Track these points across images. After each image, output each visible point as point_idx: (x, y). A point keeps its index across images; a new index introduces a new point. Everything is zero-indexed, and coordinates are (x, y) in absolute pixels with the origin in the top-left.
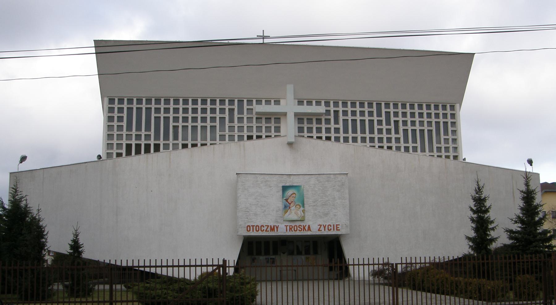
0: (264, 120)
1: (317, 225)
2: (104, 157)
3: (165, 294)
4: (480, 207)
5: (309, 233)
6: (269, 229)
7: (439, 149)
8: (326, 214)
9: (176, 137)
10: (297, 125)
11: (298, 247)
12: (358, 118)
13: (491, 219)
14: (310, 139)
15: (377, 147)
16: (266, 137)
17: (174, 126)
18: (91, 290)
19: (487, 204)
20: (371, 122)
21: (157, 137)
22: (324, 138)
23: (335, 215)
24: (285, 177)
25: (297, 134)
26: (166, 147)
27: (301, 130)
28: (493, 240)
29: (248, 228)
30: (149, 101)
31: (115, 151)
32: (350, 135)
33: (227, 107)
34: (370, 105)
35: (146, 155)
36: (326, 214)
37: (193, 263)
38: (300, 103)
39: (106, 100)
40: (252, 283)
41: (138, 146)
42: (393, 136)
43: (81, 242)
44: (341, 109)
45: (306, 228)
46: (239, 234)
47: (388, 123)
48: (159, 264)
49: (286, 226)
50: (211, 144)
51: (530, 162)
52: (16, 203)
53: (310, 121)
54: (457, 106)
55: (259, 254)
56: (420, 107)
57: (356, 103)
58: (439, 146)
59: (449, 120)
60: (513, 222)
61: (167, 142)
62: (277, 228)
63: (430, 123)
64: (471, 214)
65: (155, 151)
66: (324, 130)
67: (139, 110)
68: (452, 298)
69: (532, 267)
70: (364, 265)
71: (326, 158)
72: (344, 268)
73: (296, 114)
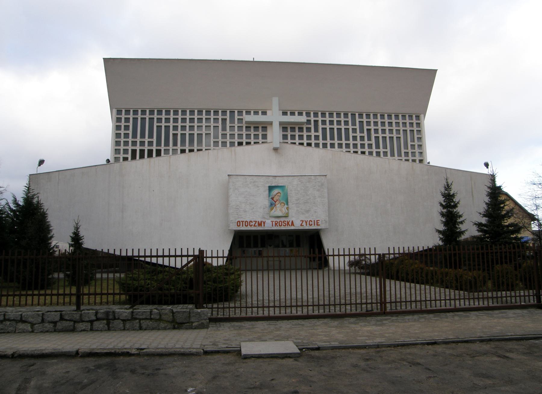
0: (252, 129)
1: (299, 221)
2: (112, 161)
3: (148, 284)
4: (449, 203)
5: (292, 228)
6: (257, 224)
7: (407, 154)
8: (308, 211)
9: (175, 144)
10: (282, 133)
11: (282, 241)
12: (335, 127)
13: (460, 214)
14: (294, 145)
15: (352, 152)
16: (255, 143)
17: (174, 134)
18: (93, 278)
19: (456, 199)
20: (347, 130)
21: (159, 143)
22: (305, 144)
23: (315, 212)
24: (271, 178)
25: (282, 141)
26: (167, 152)
27: (285, 137)
28: (462, 233)
29: (239, 223)
30: (152, 112)
31: (122, 156)
32: (329, 142)
33: (220, 117)
34: (346, 115)
35: (148, 159)
36: (308, 211)
37: (166, 253)
38: (285, 113)
39: (115, 111)
40: (236, 273)
41: (142, 151)
42: (366, 142)
43: (82, 234)
44: (320, 119)
45: (290, 223)
46: (230, 228)
47: (362, 131)
48: (160, 253)
49: (272, 222)
50: (206, 150)
51: (487, 165)
52: (28, 200)
53: (293, 129)
54: (422, 116)
55: (249, 246)
56: (390, 116)
57: (333, 114)
58: (406, 151)
59: (415, 128)
60: (482, 216)
61: (167, 148)
62: (264, 223)
63: (398, 131)
64: (440, 209)
65: (157, 156)
66: (305, 137)
67: (143, 120)
68: (427, 287)
69: (501, 258)
70: (339, 255)
71: (308, 160)
72: (323, 259)
73: (281, 123)
